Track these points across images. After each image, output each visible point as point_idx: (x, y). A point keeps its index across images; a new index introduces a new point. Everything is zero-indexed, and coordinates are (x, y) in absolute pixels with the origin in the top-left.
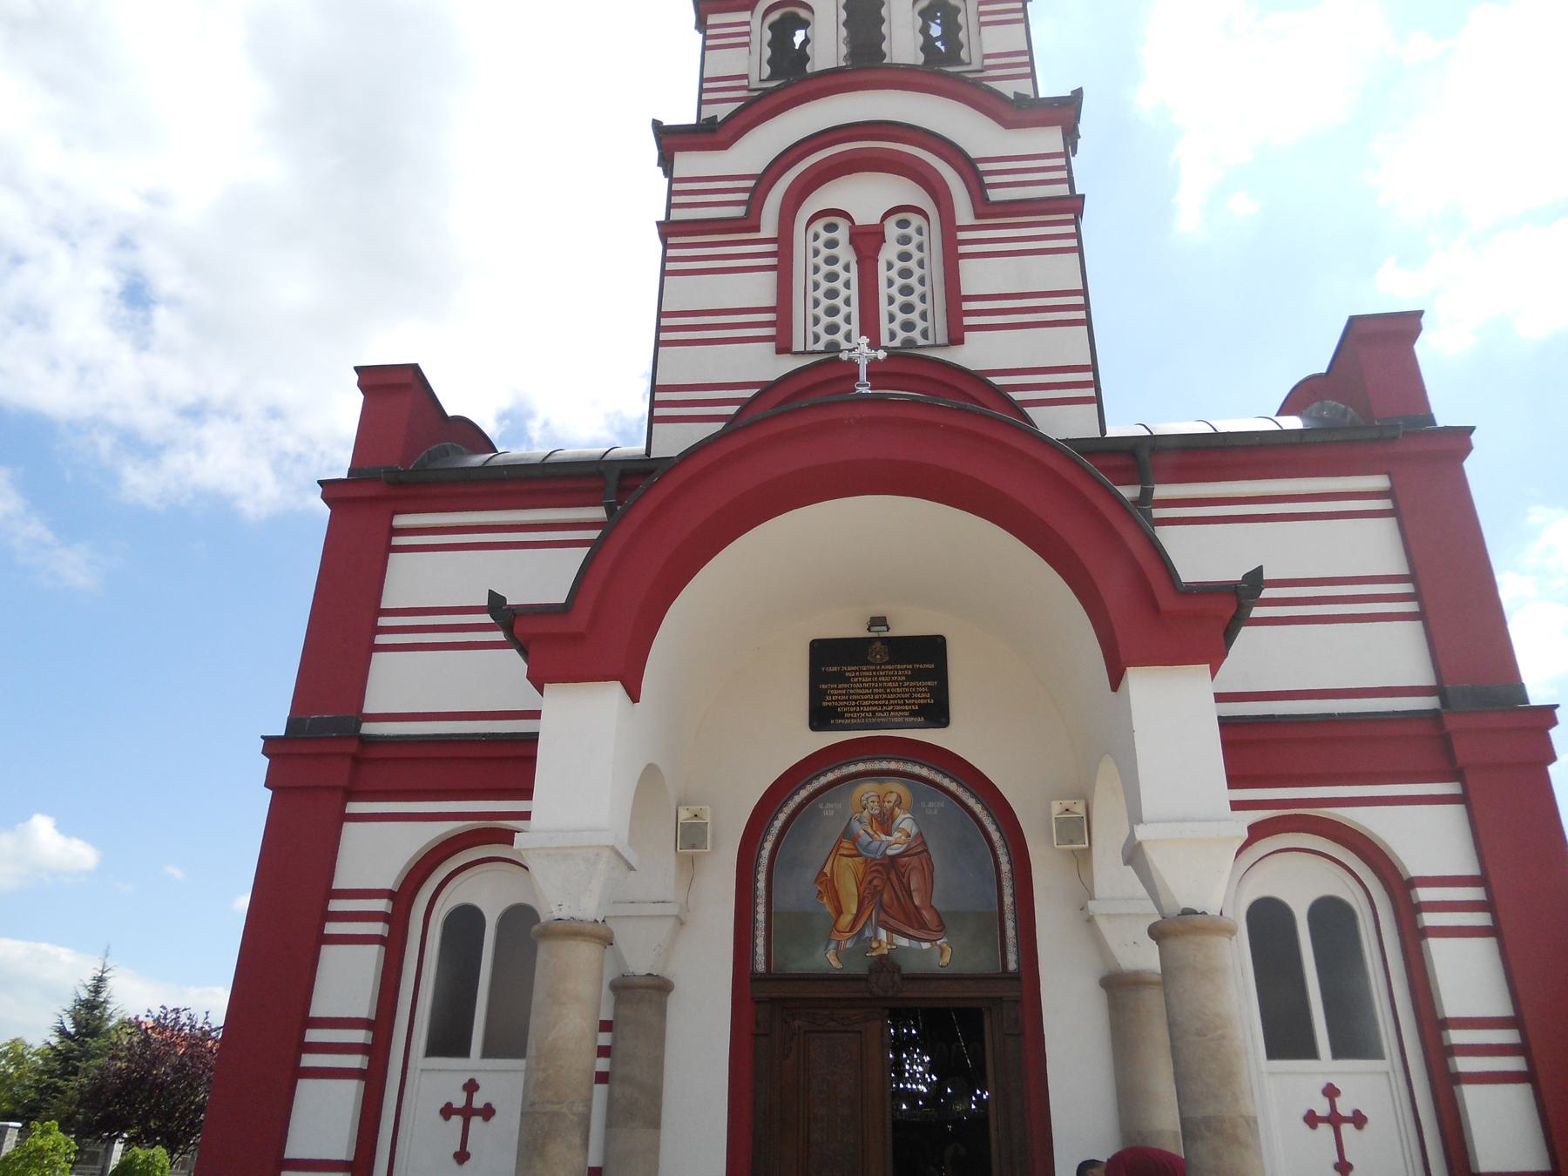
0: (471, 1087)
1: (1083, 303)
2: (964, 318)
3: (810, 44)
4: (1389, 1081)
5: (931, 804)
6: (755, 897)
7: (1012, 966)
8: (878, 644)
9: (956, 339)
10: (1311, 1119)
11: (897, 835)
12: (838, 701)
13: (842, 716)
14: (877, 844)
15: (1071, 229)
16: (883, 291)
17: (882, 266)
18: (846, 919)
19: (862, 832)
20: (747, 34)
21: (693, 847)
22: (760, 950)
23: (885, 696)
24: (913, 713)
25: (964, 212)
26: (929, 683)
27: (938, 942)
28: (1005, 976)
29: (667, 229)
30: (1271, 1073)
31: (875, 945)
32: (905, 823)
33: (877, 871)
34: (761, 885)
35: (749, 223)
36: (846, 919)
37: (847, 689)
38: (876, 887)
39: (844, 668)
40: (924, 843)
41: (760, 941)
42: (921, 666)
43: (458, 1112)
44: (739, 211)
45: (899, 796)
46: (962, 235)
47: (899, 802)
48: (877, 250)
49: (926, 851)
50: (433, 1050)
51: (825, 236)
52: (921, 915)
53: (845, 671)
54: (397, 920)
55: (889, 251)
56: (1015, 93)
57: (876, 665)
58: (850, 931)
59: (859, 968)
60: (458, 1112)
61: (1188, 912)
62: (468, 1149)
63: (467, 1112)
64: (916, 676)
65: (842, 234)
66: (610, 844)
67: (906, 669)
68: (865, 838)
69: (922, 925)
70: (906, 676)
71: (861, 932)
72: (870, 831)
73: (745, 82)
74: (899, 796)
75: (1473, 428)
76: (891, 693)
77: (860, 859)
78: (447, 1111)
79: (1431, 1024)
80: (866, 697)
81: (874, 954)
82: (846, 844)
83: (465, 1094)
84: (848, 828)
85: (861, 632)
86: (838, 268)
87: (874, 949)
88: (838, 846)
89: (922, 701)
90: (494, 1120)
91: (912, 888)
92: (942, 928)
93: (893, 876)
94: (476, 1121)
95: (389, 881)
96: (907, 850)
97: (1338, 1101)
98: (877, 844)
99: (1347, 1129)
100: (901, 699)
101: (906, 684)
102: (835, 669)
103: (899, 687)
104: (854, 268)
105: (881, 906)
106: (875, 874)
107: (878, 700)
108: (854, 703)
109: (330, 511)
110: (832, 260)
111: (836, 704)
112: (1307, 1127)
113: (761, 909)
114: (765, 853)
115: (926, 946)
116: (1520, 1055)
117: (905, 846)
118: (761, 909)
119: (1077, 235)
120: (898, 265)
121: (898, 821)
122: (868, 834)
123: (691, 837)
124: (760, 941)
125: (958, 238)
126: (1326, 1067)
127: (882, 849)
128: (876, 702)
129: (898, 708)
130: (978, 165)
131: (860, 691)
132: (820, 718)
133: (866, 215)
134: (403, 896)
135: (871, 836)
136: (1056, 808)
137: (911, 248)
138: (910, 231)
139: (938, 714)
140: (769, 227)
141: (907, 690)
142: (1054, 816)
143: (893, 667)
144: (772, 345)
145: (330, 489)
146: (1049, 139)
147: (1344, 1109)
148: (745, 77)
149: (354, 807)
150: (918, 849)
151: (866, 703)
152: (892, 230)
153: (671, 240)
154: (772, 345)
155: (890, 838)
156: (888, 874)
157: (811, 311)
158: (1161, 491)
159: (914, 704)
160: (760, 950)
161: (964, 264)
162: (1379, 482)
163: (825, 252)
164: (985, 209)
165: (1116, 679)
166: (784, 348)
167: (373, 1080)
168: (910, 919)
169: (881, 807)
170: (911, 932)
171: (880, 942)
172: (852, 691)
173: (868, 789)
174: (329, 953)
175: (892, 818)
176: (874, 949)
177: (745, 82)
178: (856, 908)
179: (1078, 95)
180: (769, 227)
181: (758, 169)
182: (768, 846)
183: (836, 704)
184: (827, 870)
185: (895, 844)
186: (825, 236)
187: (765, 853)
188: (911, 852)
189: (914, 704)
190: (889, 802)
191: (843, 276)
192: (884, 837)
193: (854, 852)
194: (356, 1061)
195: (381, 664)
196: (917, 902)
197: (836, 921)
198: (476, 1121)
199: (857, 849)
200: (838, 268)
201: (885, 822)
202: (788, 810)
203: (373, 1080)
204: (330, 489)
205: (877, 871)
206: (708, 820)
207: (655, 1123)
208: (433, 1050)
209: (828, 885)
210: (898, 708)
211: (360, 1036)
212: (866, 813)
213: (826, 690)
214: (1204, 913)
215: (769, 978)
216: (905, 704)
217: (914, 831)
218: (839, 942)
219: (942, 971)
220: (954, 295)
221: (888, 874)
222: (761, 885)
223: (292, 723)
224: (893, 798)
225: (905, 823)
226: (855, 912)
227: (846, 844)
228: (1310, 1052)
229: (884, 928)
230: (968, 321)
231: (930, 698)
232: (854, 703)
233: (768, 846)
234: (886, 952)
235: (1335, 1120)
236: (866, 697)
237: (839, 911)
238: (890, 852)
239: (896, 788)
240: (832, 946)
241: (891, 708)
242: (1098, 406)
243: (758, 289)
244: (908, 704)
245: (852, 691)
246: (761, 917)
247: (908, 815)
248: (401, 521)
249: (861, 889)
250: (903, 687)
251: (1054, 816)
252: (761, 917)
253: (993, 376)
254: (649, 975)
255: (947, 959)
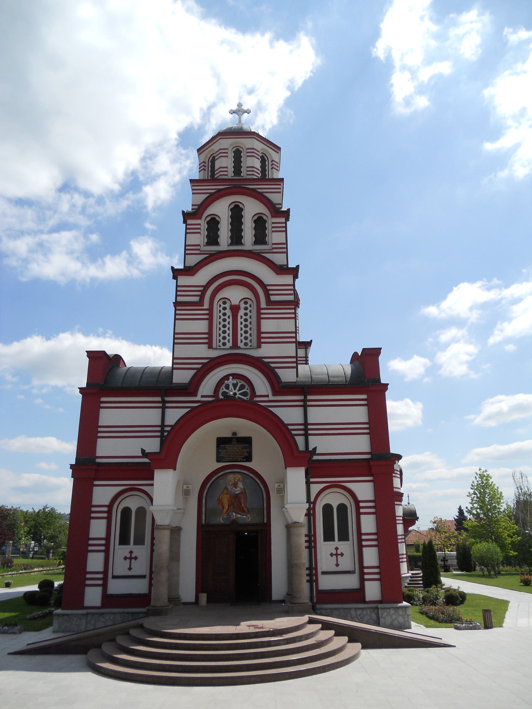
0: (131, 552)
1: (295, 336)
2: (262, 339)
3: (219, 238)
4: (350, 546)
5: (247, 480)
6: (202, 505)
7: (265, 521)
8: (234, 439)
9: (259, 346)
10: (332, 555)
11: (238, 488)
12: (224, 454)
13: (224, 459)
14: (233, 491)
15: (293, 311)
16: (239, 326)
17: (239, 317)
18: (225, 510)
19: (230, 488)
20: (200, 229)
21: (187, 495)
22: (204, 518)
23: (236, 453)
24: (243, 458)
25: (263, 305)
26: (247, 450)
27: (248, 516)
28: (263, 524)
29: (176, 304)
30: (324, 545)
31: (232, 517)
32: (240, 485)
33: (233, 498)
34: (204, 502)
35: (201, 303)
36: (225, 510)
37: (226, 451)
38: (232, 502)
39: (225, 445)
40: (245, 490)
41: (204, 516)
42: (245, 445)
43: (128, 558)
44: (196, 299)
45: (239, 478)
46: (262, 311)
47: (239, 480)
48: (238, 312)
49: (246, 493)
50: (120, 543)
51: (223, 306)
52: (243, 509)
53: (226, 446)
54: (109, 512)
55: (241, 312)
56: (289, 210)
57: (234, 445)
58: (226, 513)
59: (228, 522)
60: (128, 558)
61: (296, 522)
62: (132, 567)
63: (131, 558)
64: (244, 448)
65: (227, 306)
66: (172, 509)
67: (242, 446)
68: (230, 489)
69: (244, 512)
70: (242, 448)
71: (229, 513)
72: (231, 487)
73: (199, 247)
74: (239, 478)
75: (388, 384)
76: (237, 453)
77: (228, 495)
78: (126, 558)
79: (360, 534)
80: (231, 454)
81: (232, 519)
82: (225, 491)
83: (130, 554)
84: (226, 486)
85: (230, 435)
86: (226, 317)
87: (232, 518)
88: (223, 491)
89: (245, 455)
90: (137, 560)
91: (242, 502)
92: (249, 512)
93: (237, 499)
94: (133, 561)
95: (107, 503)
96: (241, 492)
97: (338, 550)
98: (233, 491)
99: (339, 557)
100: (240, 454)
101: (241, 450)
102: (223, 446)
103: (240, 451)
104: (231, 317)
105: (234, 507)
106: (233, 499)
107: (234, 454)
108: (228, 455)
109: (82, 395)
110: (224, 314)
111: (223, 455)
112: (330, 556)
113: (204, 508)
114: (205, 494)
115: (244, 517)
116: (376, 541)
117: (240, 491)
118: (204, 508)
119: (295, 313)
120: (244, 317)
121: (238, 485)
122: (231, 488)
123: (187, 493)
124: (204, 516)
125: (261, 312)
126: (336, 543)
127: (235, 492)
128: (234, 455)
129: (239, 457)
130: (267, 287)
131: (229, 452)
132: (219, 460)
133: (235, 301)
134: (110, 506)
135: (232, 489)
136: (276, 485)
137: (248, 311)
138: (248, 306)
139: (249, 458)
140: (206, 305)
141: (242, 452)
142: (276, 487)
143: (238, 445)
144: (207, 345)
145: (81, 390)
146: (287, 279)
147: (339, 552)
148: (199, 245)
149: (96, 483)
150: (243, 492)
151: (231, 455)
152: (243, 306)
153: (177, 308)
154: (207, 345)
155: (236, 489)
156: (236, 499)
157: (218, 332)
158: (309, 397)
159: (243, 456)
160: (204, 518)
161: (262, 321)
162: (364, 396)
163: (223, 311)
164: (269, 302)
165: (286, 469)
166: (210, 347)
167: (107, 552)
168: (241, 510)
169: (234, 481)
170: (242, 513)
171: (233, 516)
172: (227, 452)
173: (231, 477)
174: (93, 522)
175: (237, 484)
176: (232, 518)
177: (199, 247)
178: (227, 507)
179: (298, 267)
180: (206, 305)
181: (204, 284)
182: (206, 492)
183: (223, 455)
184: (220, 498)
185: (238, 491)
186: (223, 306)
187: (205, 494)
188: (242, 493)
189: (243, 456)
190: (237, 480)
191: (228, 320)
192: (235, 489)
193: (227, 493)
194: (103, 548)
195: (100, 441)
196: (243, 506)
197: (223, 511)
198: (133, 561)
199: (228, 492)
200: (226, 317)
201: (235, 485)
202: (211, 482)
203: (107, 552)
204: (81, 390)
205: (233, 498)
206: (191, 488)
207: (179, 561)
208: (120, 543)
209: (220, 501)
210: (239, 457)
211: (103, 542)
212: (231, 483)
213: (221, 451)
214: (299, 523)
215: (207, 525)
216: (241, 456)
217: (242, 487)
218: (223, 516)
219: (248, 523)
220: (259, 332)
221: (236, 499)
222: (204, 502)
223: (77, 459)
224: (237, 479)
225: (240, 485)
226: (227, 508)
227: (225, 491)
228: (333, 540)
229: (234, 512)
230: (263, 340)
231: (247, 454)
232: (228, 455)
233: (206, 492)
234: (235, 518)
235: (337, 555)
236: (231, 454)
237: (223, 508)
238: (236, 493)
239: (239, 476)
240: (221, 517)
241: (237, 457)
242: (296, 369)
243: (202, 326)
244: (242, 456)
245: (227, 452)
246: (204, 510)
247: (241, 483)
248: (103, 399)
249: (229, 502)
250: (240, 451)
251: (276, 487)
252: (204, 510)
253: (260, 402)
254: (176, 527)
255: (250, 520)
